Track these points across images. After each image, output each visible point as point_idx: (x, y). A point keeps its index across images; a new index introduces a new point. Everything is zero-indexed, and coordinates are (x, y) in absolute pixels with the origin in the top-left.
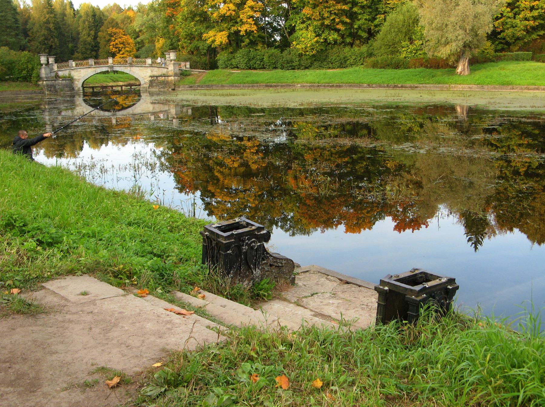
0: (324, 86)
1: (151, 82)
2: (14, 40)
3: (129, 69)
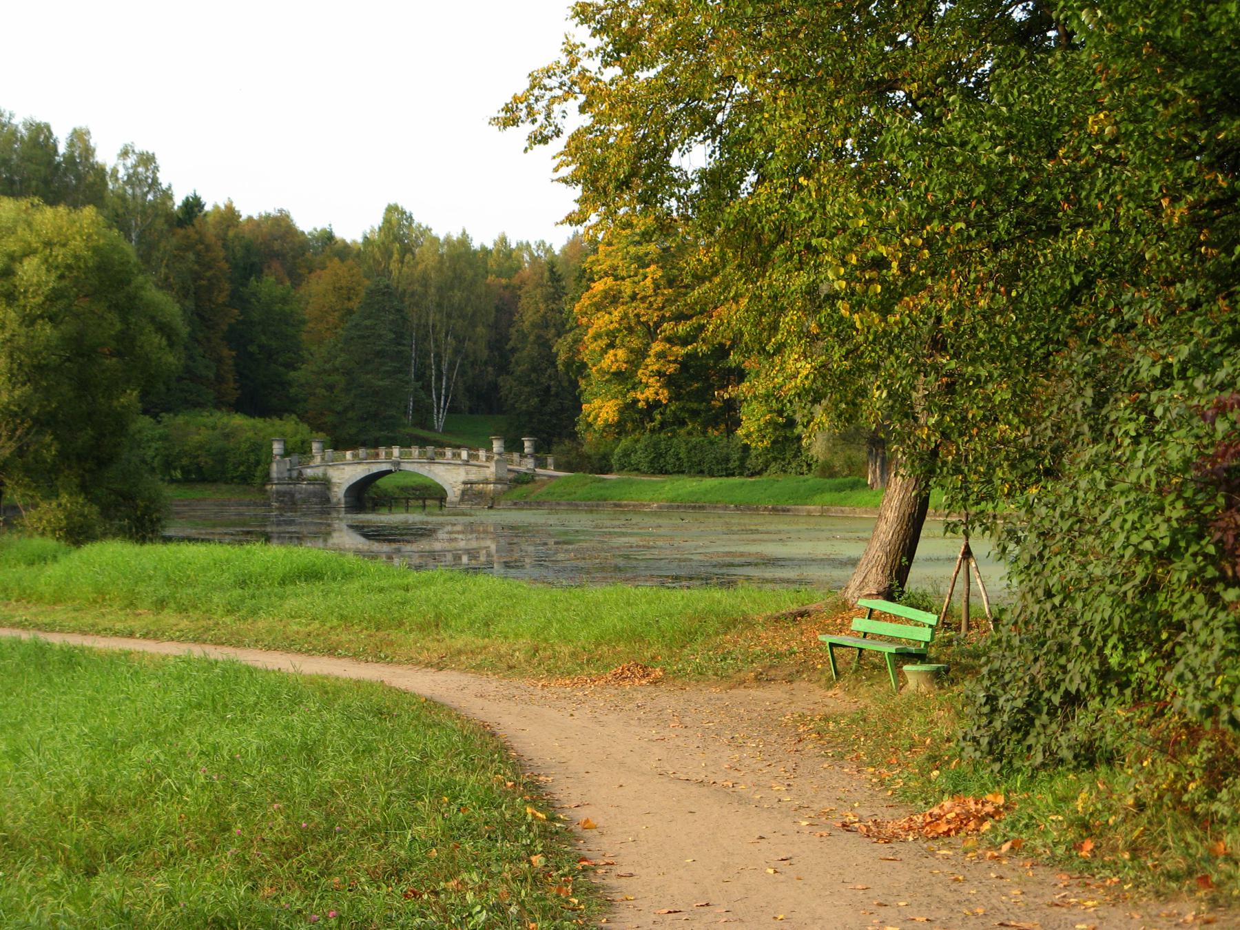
1: (464, 493)
2: (386, 383)
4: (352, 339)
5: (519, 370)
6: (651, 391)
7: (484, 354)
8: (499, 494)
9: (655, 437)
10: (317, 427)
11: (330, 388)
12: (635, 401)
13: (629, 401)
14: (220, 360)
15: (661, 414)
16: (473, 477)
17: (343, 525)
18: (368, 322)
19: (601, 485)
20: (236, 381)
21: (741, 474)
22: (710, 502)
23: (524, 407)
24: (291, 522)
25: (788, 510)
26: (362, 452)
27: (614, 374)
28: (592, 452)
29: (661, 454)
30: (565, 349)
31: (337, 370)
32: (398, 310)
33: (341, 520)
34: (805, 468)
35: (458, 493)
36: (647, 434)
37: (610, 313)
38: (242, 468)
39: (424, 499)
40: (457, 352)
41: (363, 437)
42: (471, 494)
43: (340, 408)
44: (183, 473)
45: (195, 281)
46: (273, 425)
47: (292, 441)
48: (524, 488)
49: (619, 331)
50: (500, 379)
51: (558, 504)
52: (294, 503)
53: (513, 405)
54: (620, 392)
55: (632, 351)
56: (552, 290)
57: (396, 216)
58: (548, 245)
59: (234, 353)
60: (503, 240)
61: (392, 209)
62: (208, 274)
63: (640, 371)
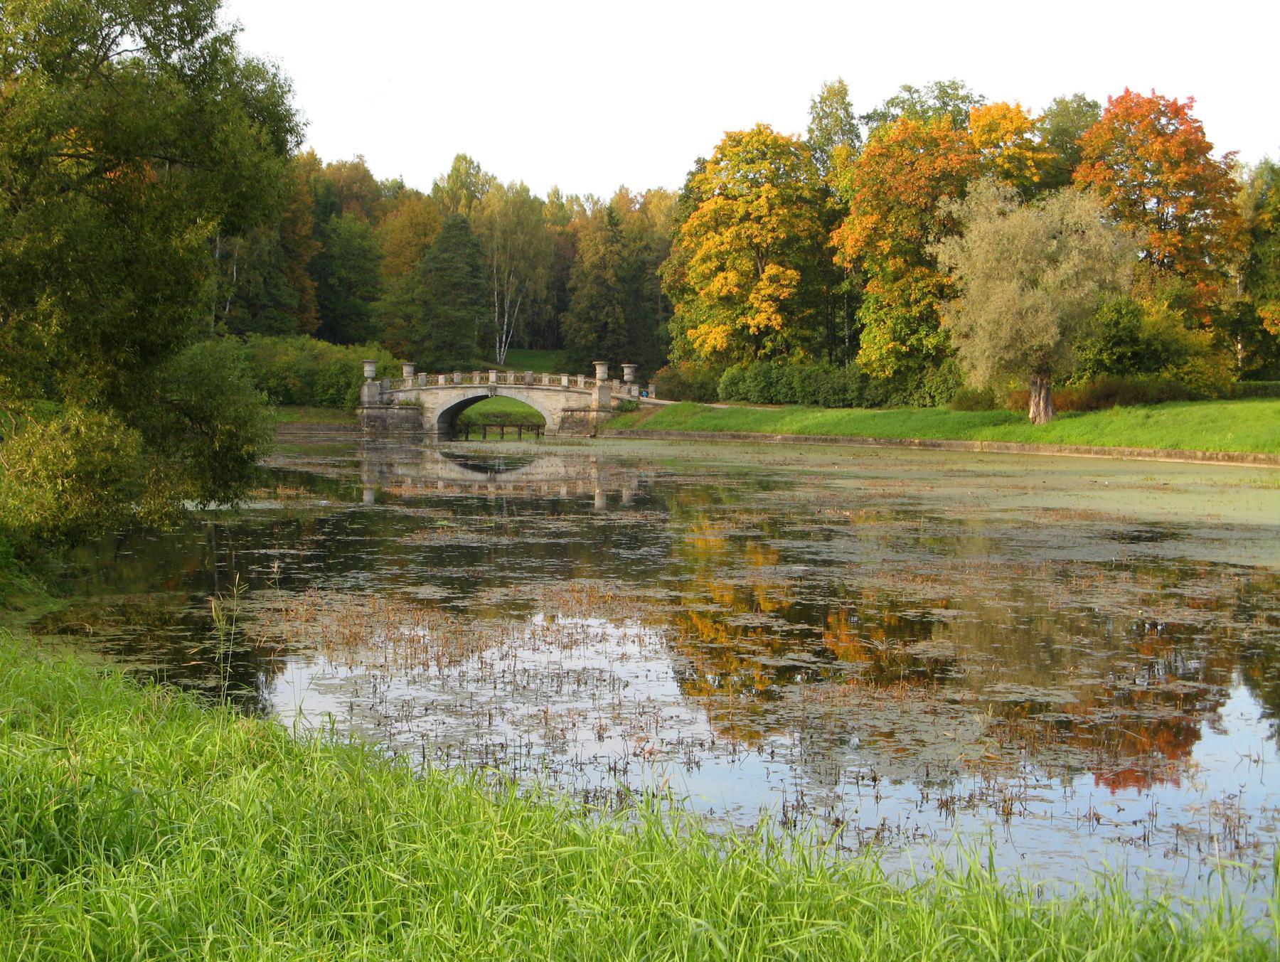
0: (814, 440)
1: (563, 420)
2: (463, 313)
5: (579, 308)
6: (762, 316)
7: (544, 294)
9: (765, 365)
11: (408, 318)
13: (738, 326)
14: (303, 291)
16: (573, 405)
18: (446, 256)
19: (712, 414)
20: (317, 311)
21: (859, 405)
22: (844, 435)
23: (583, 342)
25: (939, 446)
26: (457, 376)
27: (721, 299)
29: (771, 384)
34: (928, 400)
35: (558, 420)
37: (721, 234)
38: (331, 391)
39: (502, 426)
40: (519, 291)
41: (439, 366)
42: (572, 421)
46: (356, 352)
48: (629, 417)
49: (729, 253)
51: (669, 434)
52: (385, 428)
53: (572, 340)
57: (463, 168)
59: (316, 284)
61: (461, 159)
62: (293, 207)
63: (752, 296)
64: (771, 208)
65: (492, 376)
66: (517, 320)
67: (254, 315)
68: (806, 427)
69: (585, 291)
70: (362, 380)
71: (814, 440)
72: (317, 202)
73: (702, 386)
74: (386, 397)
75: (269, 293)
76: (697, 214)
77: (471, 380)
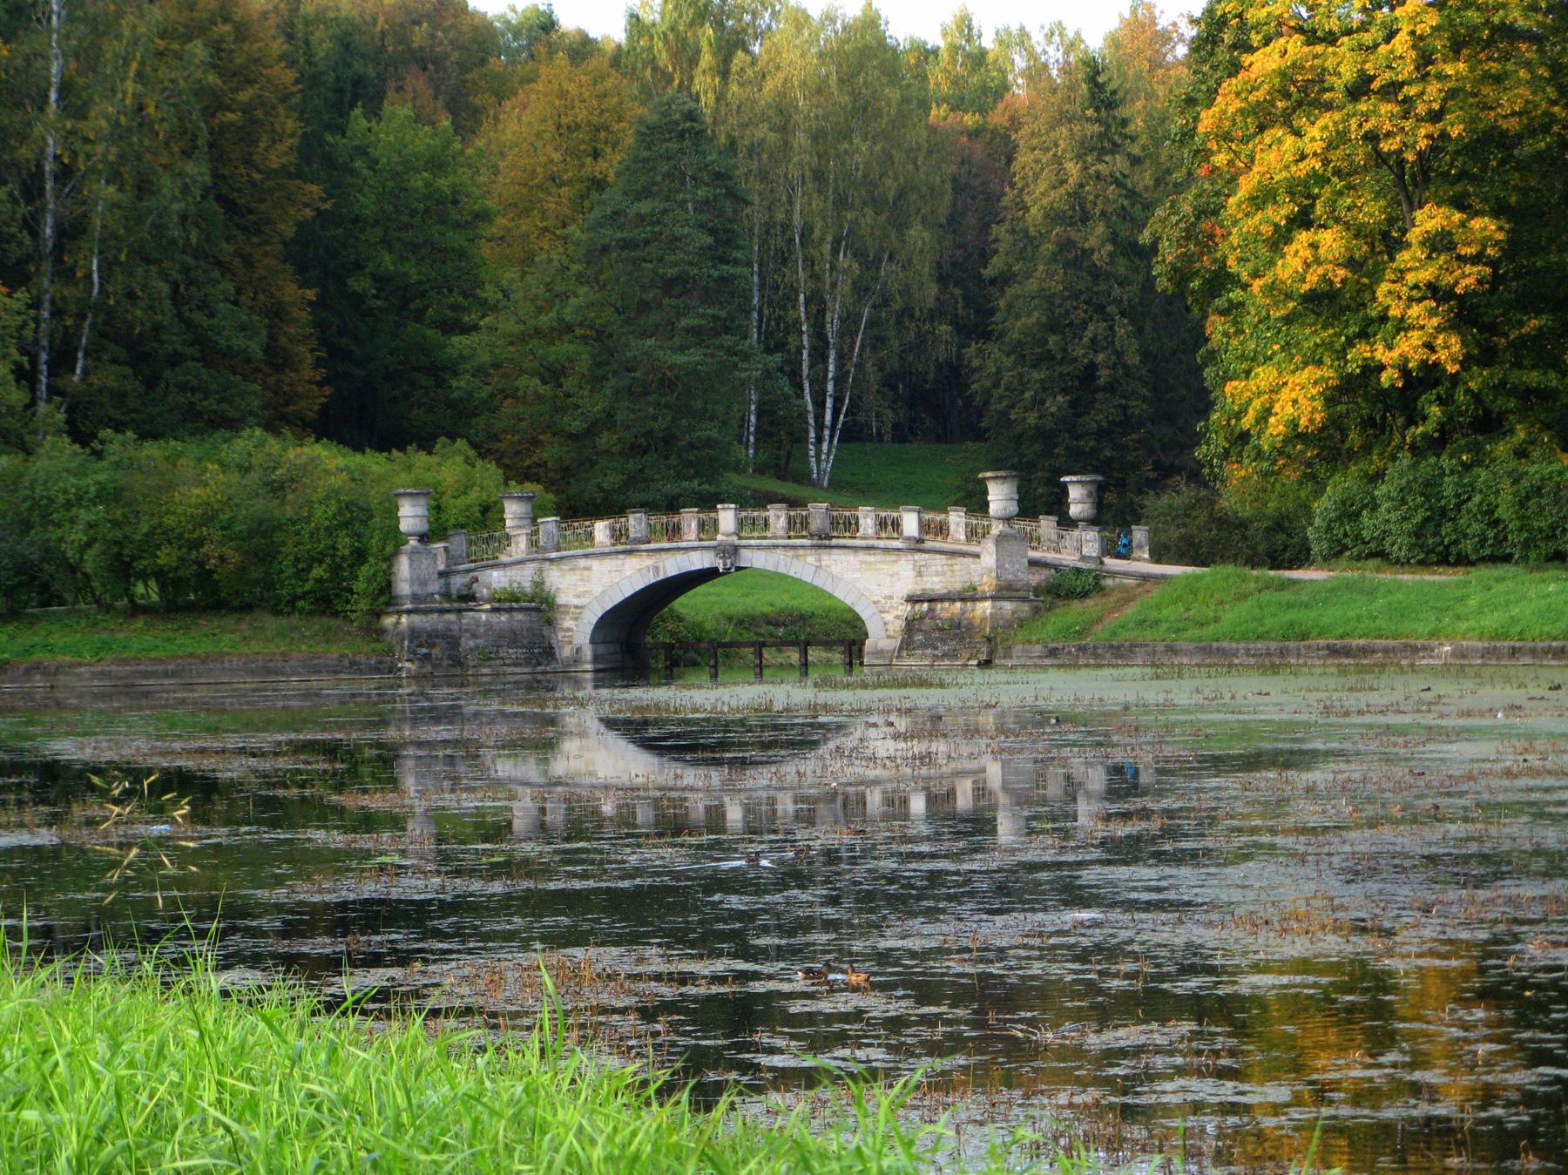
0: (1533, 652)
1: (911, 625)
2: (694, 356)
3: (811, 559)
4: (605, 249)
5: (1017, 328)
8: (1009, 626)
9: (1428, 465)
10: (518, 471)
11: (554, 374)
12: (1372, 369)
14: (277, 313)
15: (1441, 401)
17: (590, 719)
18: (644, 207)
19: (1287, 596)
23: (1032, 419)
24: (449, 715)
26: (636, 523)
28: (1246, 512)
29: (1443, 512)
30: (1177, 233)
31: (569, 329)
32: (719, 176)
33: (582, 704)
35: (899, 625)
36: (1405, 459)
37: (1298, 134)
38: (318, 572)
40: (861, 289)
43: (577, 425)
44: (163, 587)
45: (209, 113)
46: (409, 468)
47: (455, 508)
48: (1075, 611)
49: (1322, 180)
50: (971, 351)
51: (1172, 650)
52: (458, 662)
53: (1004, 414)
54: (1328, 346)
55: (1359, 232)
56: (1096, 128)
58: (1070, 34)
59: (311, 294)
60: (965, 25)
62: (244, 96)
63: (1383, 288)
64: (1425, 59)
65: (727, 517)
66: (859, 366)
67: (151, 384)
68: (1514, 621)
69: (1032, 285)
70: (395, 538)
71: (1533, 652)
72: (311, 81)
73: (1281, 525)
74: (458, 582)
75: (188, 323)
76: (1235, 83)
77: (675, 532)
